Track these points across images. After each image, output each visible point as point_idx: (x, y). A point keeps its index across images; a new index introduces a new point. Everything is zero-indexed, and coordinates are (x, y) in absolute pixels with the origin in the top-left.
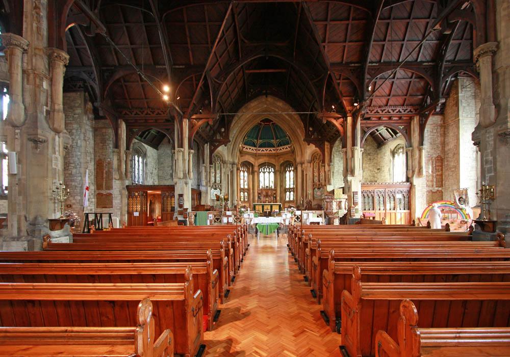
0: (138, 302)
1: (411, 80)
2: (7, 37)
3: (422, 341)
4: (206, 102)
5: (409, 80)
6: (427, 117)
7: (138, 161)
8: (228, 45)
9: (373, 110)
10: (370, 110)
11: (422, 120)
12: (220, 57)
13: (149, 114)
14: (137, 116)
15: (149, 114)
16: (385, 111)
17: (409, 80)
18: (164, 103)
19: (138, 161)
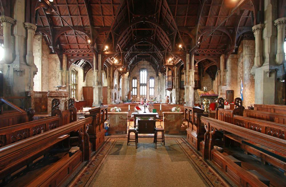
0: (52, 116)
1: (221, 35)
2: (230, 161)
3: (111, 23)
4: (90, 67)
5: (220, 35)
6: (228, 55)
7: (21, 111)
8: (167, 13)
9: (201, 51)
10: (199, 51)
11: (226, 57)
12: (167, 13)
13: (86, 52)
14: (73, 53)
15: (74, 52)
16: (207, 51)
17: (220, 35)
18: (109, 46)
19: (21, 111)
